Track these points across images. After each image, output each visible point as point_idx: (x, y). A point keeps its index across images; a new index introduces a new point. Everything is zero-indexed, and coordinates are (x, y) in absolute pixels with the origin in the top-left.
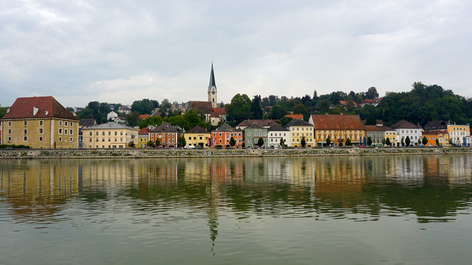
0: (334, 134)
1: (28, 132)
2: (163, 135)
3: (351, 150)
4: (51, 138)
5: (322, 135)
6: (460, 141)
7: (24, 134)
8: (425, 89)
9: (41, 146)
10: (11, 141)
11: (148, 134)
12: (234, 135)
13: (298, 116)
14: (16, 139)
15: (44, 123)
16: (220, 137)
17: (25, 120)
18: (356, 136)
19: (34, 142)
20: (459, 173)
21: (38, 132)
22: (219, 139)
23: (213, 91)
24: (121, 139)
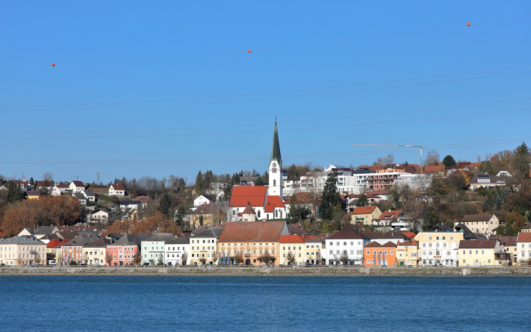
0: (259, 247)
3: (468, 224)
5: (270, 248)
6: (441, 257)
11: (61, 248)
12: (127, 250)
13: (153, 243)
18: (229, 249)
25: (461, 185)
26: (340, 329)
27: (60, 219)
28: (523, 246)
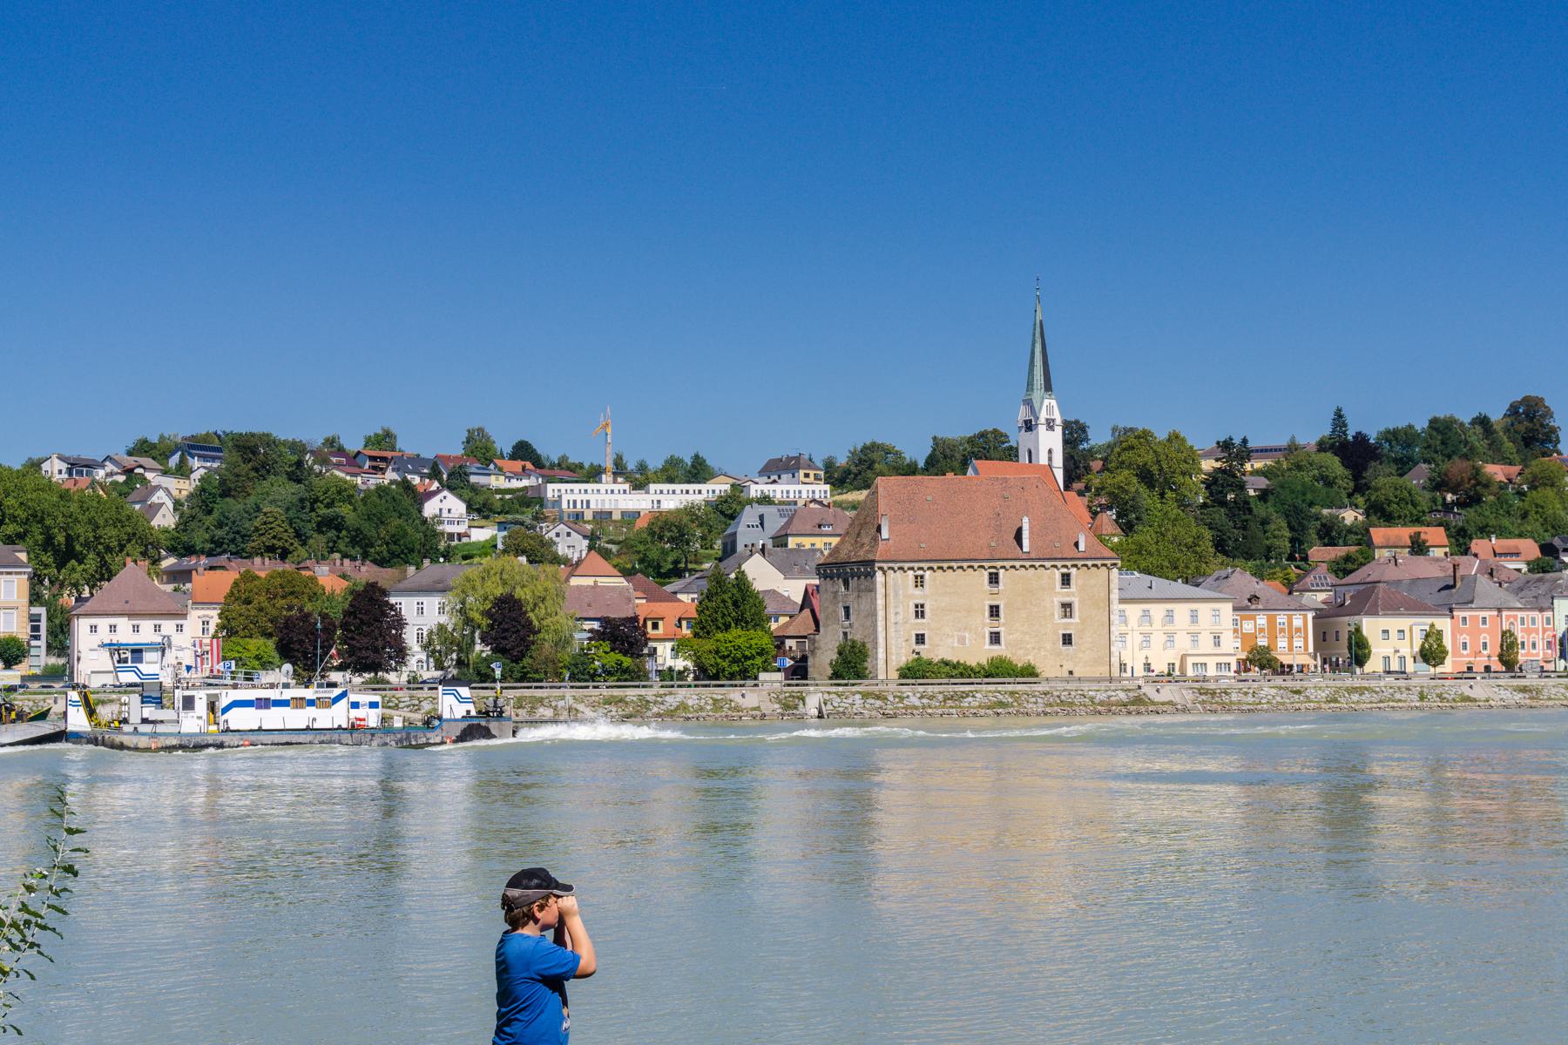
3: (743, 696)
4: (1113, 638)
7: (988, 621)
9: (1068, 666)
12: (1528, 623)
14: (950, 640)
15: (1080, 582)
16: (1485, 631)
17: (990, 568)
20: (377, 763)
21: (1053, 614)
22: (1481, 637)
23: (1048, 417)
24: (1215, 637)
28: (1194, 616)
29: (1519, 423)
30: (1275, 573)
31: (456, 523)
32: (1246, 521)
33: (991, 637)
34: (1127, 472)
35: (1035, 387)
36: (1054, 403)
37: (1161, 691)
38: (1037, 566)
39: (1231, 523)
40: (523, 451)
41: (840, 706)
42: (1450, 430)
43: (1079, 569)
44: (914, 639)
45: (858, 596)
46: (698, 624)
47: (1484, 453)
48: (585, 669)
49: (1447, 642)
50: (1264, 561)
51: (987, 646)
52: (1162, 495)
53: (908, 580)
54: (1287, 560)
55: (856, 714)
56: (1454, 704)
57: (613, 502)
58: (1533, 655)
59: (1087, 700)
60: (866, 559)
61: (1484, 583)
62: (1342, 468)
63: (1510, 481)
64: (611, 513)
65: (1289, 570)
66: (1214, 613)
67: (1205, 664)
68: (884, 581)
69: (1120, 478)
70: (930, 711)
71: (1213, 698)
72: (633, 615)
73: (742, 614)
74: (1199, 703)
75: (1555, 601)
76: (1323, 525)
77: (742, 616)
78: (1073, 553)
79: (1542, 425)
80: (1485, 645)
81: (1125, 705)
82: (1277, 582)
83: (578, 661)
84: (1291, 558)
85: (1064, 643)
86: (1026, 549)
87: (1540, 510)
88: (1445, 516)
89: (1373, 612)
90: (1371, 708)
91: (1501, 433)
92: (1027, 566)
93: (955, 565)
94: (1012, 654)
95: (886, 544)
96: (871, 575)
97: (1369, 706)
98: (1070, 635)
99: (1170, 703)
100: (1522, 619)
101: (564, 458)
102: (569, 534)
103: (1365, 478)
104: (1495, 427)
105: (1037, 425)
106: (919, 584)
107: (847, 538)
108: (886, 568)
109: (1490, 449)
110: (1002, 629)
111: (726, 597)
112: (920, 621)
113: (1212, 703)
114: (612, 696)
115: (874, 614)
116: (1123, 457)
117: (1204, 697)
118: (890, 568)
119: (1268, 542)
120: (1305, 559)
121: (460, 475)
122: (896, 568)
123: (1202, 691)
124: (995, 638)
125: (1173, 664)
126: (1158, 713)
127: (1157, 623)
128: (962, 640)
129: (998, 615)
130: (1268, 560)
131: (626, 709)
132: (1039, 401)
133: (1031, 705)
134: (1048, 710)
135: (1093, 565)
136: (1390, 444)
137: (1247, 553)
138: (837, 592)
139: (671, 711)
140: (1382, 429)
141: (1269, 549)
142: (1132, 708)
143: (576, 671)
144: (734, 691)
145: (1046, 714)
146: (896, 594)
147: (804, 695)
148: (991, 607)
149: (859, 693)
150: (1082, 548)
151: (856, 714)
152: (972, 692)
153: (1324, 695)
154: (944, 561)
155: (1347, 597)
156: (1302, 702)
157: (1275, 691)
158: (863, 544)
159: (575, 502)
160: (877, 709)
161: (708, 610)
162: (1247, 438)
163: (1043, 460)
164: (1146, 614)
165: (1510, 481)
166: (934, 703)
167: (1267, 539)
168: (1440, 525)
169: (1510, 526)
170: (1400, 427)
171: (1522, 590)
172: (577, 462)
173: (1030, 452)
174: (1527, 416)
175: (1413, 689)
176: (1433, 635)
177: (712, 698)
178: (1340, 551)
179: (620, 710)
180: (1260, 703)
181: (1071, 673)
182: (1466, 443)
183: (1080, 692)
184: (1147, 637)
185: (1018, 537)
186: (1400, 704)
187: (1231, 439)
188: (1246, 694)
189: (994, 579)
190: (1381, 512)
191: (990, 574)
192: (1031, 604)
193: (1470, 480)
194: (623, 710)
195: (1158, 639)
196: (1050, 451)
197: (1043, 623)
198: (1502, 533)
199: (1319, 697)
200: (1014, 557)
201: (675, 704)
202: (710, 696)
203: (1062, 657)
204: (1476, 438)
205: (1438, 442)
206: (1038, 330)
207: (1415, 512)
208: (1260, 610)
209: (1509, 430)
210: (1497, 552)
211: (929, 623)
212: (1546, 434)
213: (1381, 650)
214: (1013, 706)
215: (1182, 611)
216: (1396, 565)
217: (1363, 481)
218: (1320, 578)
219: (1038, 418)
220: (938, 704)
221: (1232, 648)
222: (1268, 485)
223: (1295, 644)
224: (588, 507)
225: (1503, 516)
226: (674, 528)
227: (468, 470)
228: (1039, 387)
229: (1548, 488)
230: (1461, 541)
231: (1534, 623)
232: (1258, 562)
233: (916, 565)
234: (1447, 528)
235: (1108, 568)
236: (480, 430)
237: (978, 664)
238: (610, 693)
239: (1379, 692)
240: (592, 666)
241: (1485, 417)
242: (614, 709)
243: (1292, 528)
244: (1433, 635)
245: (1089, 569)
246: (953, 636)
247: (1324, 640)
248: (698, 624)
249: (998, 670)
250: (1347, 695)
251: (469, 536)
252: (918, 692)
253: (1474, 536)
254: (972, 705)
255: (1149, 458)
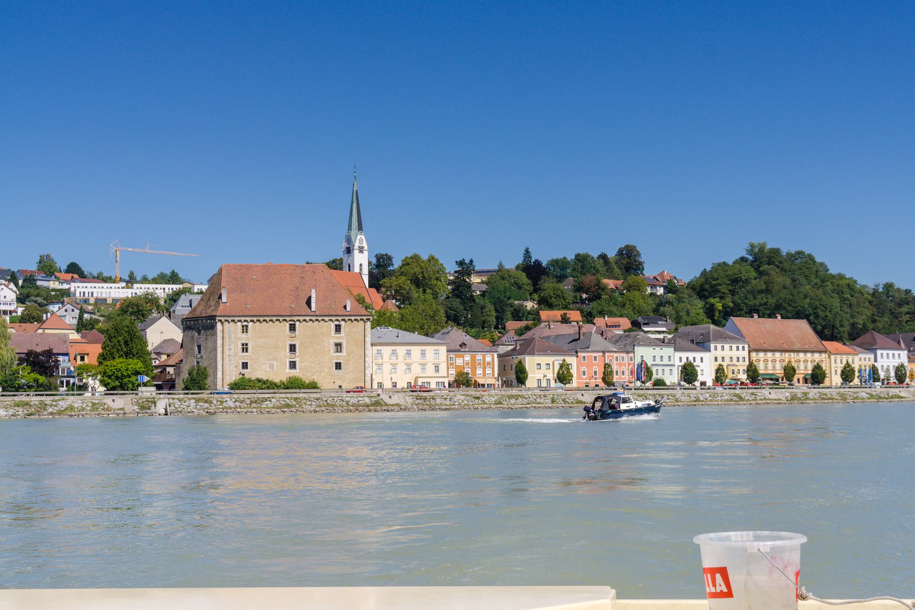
1: (299, 350)
2: (450, 358)
7: (288, 354)
8: (785, 257)
9: (338, 383)
10: (249, 370)
12: (620, 361)
14: (264, 366)
17: (290, 321)
19: (318, 373)
23: (360, 245)
24: (436, 367)
25: (730, 291)
26: (116, 526)
27: (190, 294)
28: (423, 354)
29: (623, 259)
30: (485, 335)
31: (9, 304)
32: (472, 306)
33: (290, 364)
34: (404, 278)
35: (352, 228)
36: (363, 237)
37: (392, 397)
38: (320, 320)
39: (463, 308)
40: (74, 269)
41: (179, 407)
42: (586, 260)
43: (346, 322)
44: (241, 365)
45: (206, 339)
46: (102, 356)
47: (604, 274)
48: (12, 384)
49: (574, 371)
50: (481, 329)
51: (288, 370)
52: (424, 291)
53: (237, 328)
54: (494, 329)
55: (189, 412)
56: (572, 405)
57: (108, 293)
58: (623, 379)
59: (344, 403)
60: (211, 315)
61: (596, 338)
62: (527, 279)
63: (617, 288)
64: (106, 299)
65: (494, 334)
66: (435, 352)
67: (429, 383)
68: (222, 329)
69: (401, 281)
70: (239, 410)
71: (425, 402)
72: (49, 349)
73: (130, 350)
74: (416, 405)
75: (635, 348)
76: (515, 310)
77: (130, 351)
78: (343, 312)
79: (635, 261)
80: (595, 372)
81: (368, 406)
82: (486, 340)
83: (8, 379)
84: (496, 327)
85: (336, 368)
86: (313, 309)
87: (632, 303)
88: (581, 305)
89: (532, 353)
90: (521, 408)
91: (614, 264)
92: (314, 320)
93: (268, 319)
94: (303, 375)
95: (225, 306)
96: (213, 327)
97: (520, 406)
98: (340, 363)
99: (398, 405)
100: (617, 358)
101: (100, 274)
102: (73, 310)
103: (539, 285)
104: (610, 260)
105: (353, 249)
106: (245, 331)
107: (202, 302)
108: (223, 320)
109: (607, 272)
110: (297, 360)
111: (120, 339)
112: (245, 354)
113: (423, 405)
114: (21, 401)
115: (215, 349)
116: (403, 270)
117: (419, 401)
118: (226, 321)
119: (483, 319)
120: (504, 328)
121: (30, 280)
122: (230, 321)
123: (418, 397)
124: (293, 365)
125: (410, 383)
126: (388, 411)
127: (401, 358)
128: (271, 366)
129: (295, 351)
130: (483, 328)
131: (30, 410)
132: (355, 236)
133: (307, 406)
134: (317, 409)
135: (355, 320)
136: (554, 268)
137: (471, 324)
138: (193, 336)
139: (62, 411)
140: (550, 259)
141: (484, 322)
142: (372, 408)
143: (6, 385)
144: (108, 398)
145: (315, 412)
146: (230, 337)
147: (156, 400)
148: (291, 345)
149: (194, 398)
150: (348, 309)
151: (189, 412)
152: (269, 398)
153: (494, 400)
154: (261, 317)
155: (518, 345)
156: (479, 404)
157: (464, 397)
158: (210, 306)
159: (84, 293)
160: (204, 409)
161: (108, 347)
162: (473, 259)
163: (357, 270)
164: (394, 352)
165: (617, 288)
166: (243, 405)
167: (483, 317)
168: (578, 310)
169: (616, 311)
170: (559, 259)
171: (618, 342)
172: (108, 276)
173: (349, 266)
174: (627, 255)
175: (548, 396)
176: (564, 366)
177: (91, 402)
178: (523, 324)
179: (25, 410)
180: (454, 405)
181: (340, 387)
182: (595, 268)
183: (340, 398)
184: (394, 366)
185: (309, 303)
186: (539, 405)
187: (464, 260)
188: (446, 399)
189: (293, 328)
190: (546, 303)
191: (290, 325)
192: (316, 344)
193: (595, 286)
194: (28, 411)
195: (401, 367)
196: (361, 265)
197: (323, 355)
198: (611, 314)
199: (491, 401)
200: (305, 314)
201: (65, 406)
202: (90, 400)
203: (334, 377)
204: (600, 265)
205: (580, 267)
206: (355, 195)
207: (564, 303)
208: (467, 351)
209: (617, 263)
210: (608, 324)
211: (250, 356)
212: (637, 265)
213: (536, 375)
214: (295, 407)
215: (416, 350)
216: (549, 328)
217: (538, 287)
218: (510, 338)
219: (354, 246)
220: (246, 406)
221: (447, 375)
222: (487, 289)
223: (487, 372)
224: (92, 296)
225: (612, 306)
226: (134, 306)
227: (35, 278)
228: (355, 228)
229: (637, 292)
230: (589, 318)
231: (623, 360)
232: (477, 329)
233: (243, 319)
234: (582, 312)
235: (364, 322)
236: (48, 256)
237: (281, 381)
238: (19, 399)
239: (527, 398)
240: (17, 382)
241: (605, 254)
242: (21, 410)
243: (497, 311)
244: (564, 366)
245: (352, 322)
246: (266, 363)
247: (504, 370)
248: (102, 356)
249: (293, 385)
250: (508, 400)
251: (17, 312)
252: (234, 398)
253: (596, 316)
254: (269, 406)
255: (417, 270)
